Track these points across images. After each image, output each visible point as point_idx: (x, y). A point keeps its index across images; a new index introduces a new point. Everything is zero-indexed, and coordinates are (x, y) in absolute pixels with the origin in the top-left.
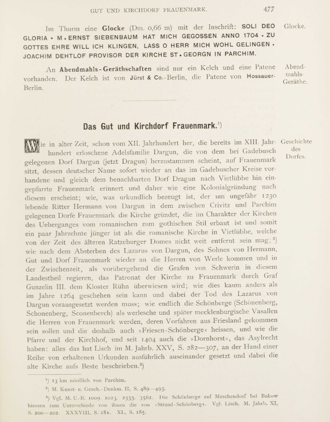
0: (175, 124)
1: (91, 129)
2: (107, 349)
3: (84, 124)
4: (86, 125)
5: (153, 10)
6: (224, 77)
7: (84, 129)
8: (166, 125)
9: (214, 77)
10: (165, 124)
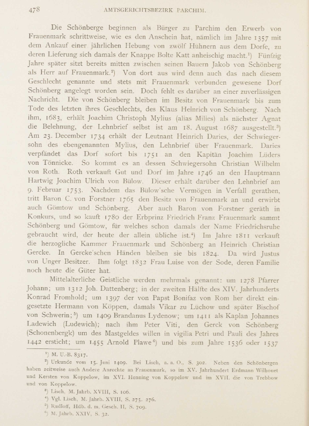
5: (110, 10)
6: (136, 281)
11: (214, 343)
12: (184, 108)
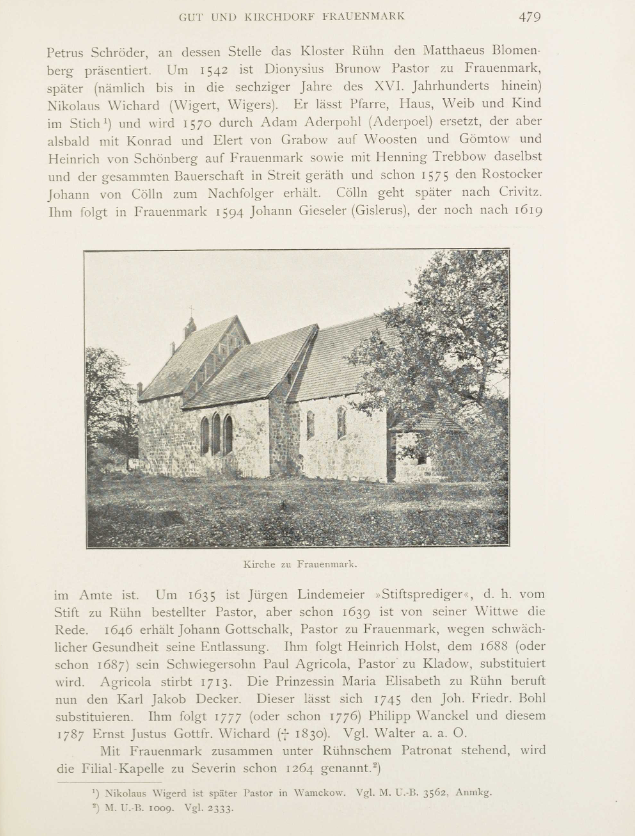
2: (181, 666)
5: (302, 17)
11: (425, 87)
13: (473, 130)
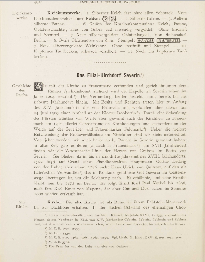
0: (89, 74)
1: (81, 77)
3: (77, 74)
4: (78, 74)
7: (77, 77)
8: (120, 75)
9: (178, 24)
10: (119, 74)
12: (115, 150)
13: (72, 159)
